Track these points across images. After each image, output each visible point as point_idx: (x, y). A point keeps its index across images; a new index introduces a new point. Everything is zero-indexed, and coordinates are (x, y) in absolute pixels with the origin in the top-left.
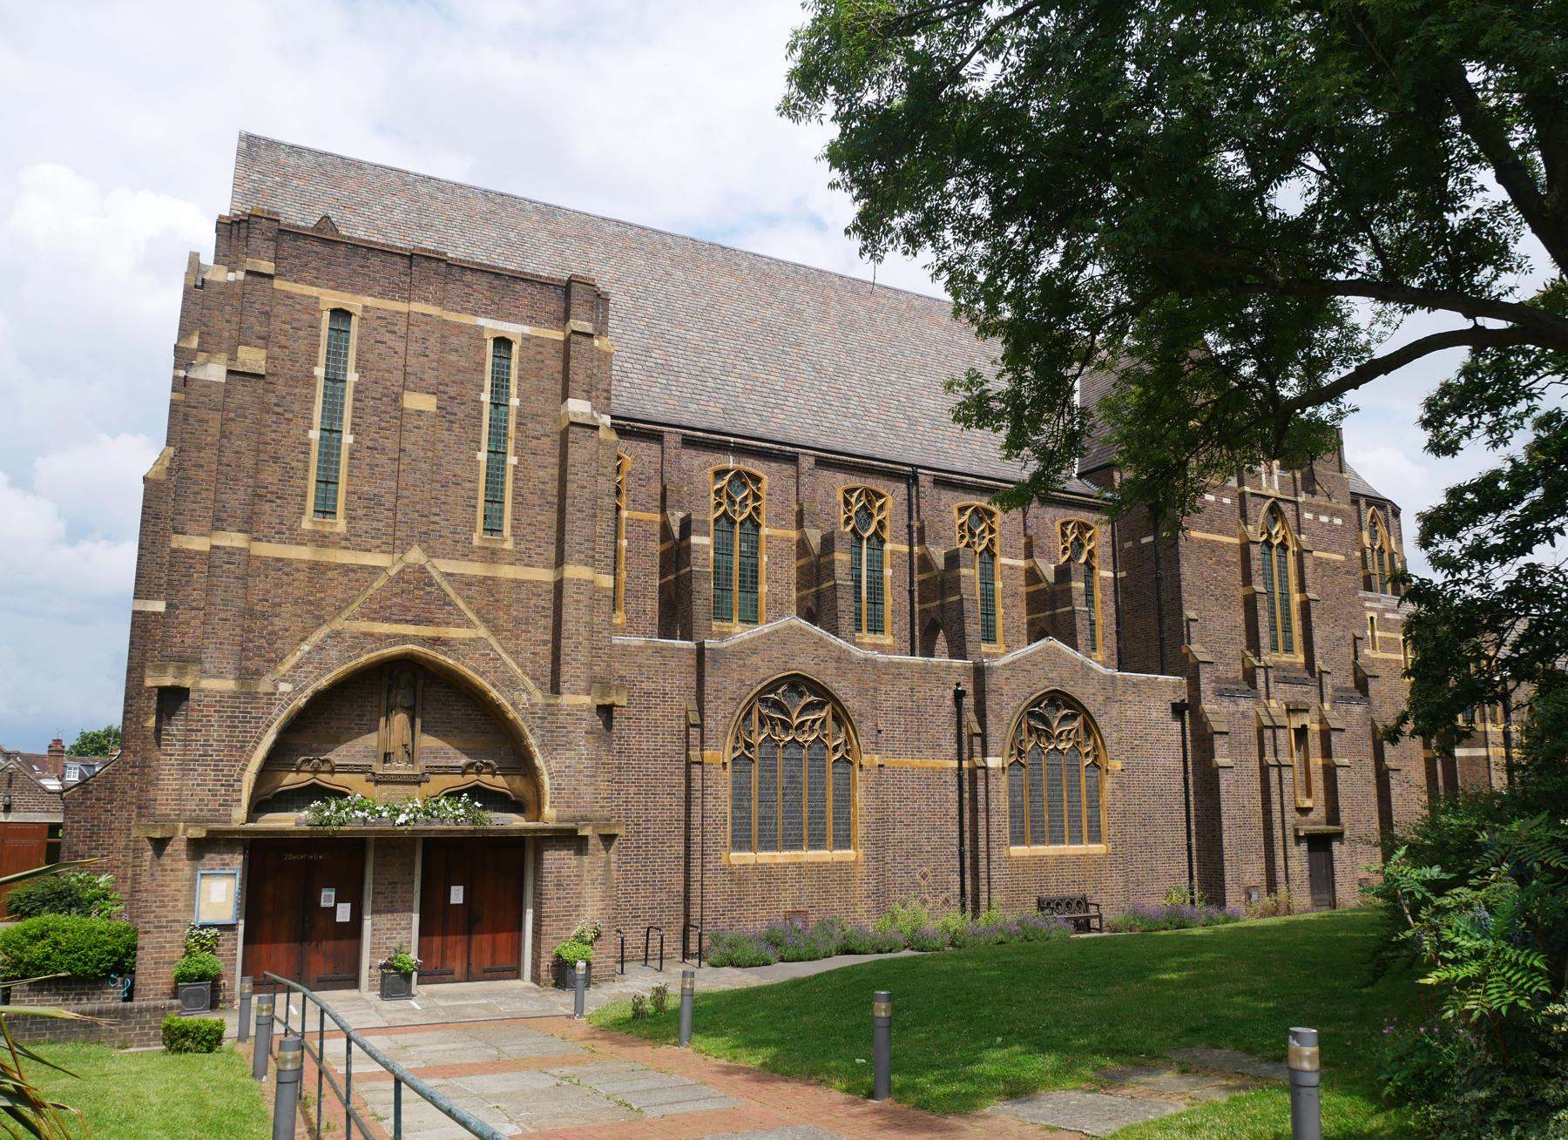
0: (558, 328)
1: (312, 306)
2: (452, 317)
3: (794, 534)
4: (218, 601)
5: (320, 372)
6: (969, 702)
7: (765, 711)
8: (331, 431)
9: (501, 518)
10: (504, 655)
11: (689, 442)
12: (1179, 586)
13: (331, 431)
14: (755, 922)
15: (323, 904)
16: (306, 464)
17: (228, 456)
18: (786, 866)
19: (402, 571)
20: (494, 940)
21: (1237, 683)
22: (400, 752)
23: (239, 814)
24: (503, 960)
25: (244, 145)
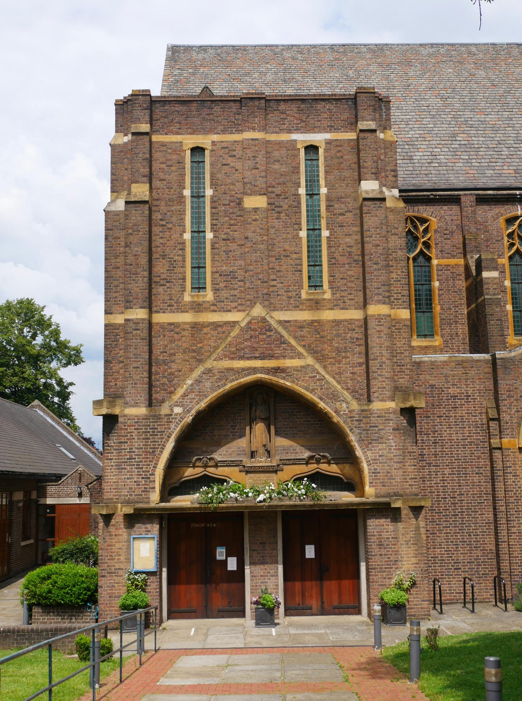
0: (352, 130)
1: (178, 148)
2: (273, 137)
4: (132, 355)
5: (187, 193)
8: (198, 232)
9: (321, 277)
10: (327, 376)
11: (482, 200)
13: (198, 232)
15: (218, 558)
16: (184, 257)
17: (131, 259)
19: (250, 323)
20: (340, 585)
22: (261, 450)
23: (155, 497)
25: (170, 53)
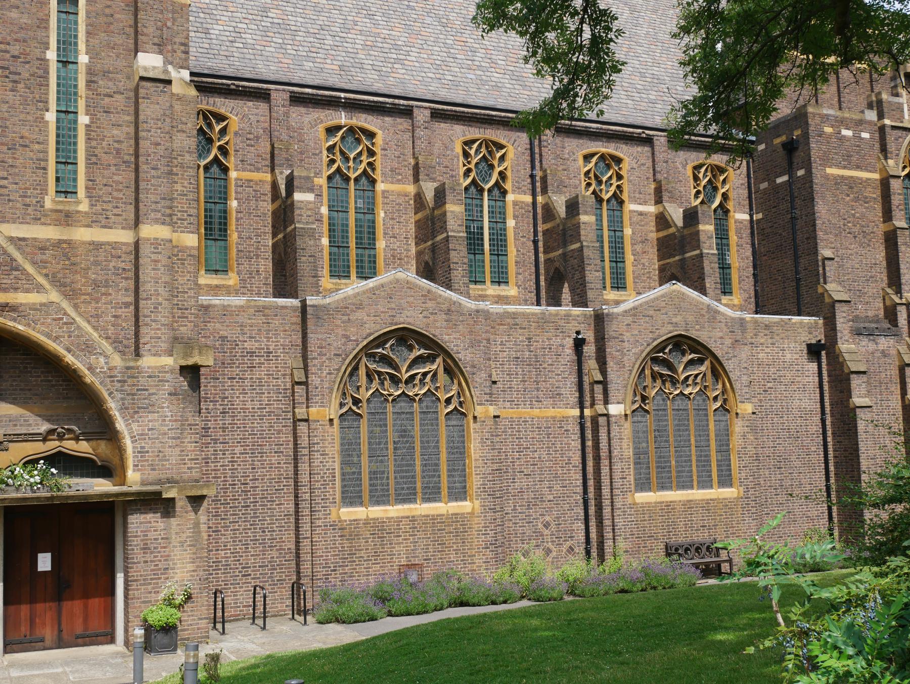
3: (411, 189)
6: (590, 350)
7: (372, 366)
9: (75, 180)
10: (78, 319)
11: (297, 100)
12: (814, 225)
14: (367, 576)
18: (399, 520)
20: (86, 607)
21: (877, 322)
24: (96, 625)
